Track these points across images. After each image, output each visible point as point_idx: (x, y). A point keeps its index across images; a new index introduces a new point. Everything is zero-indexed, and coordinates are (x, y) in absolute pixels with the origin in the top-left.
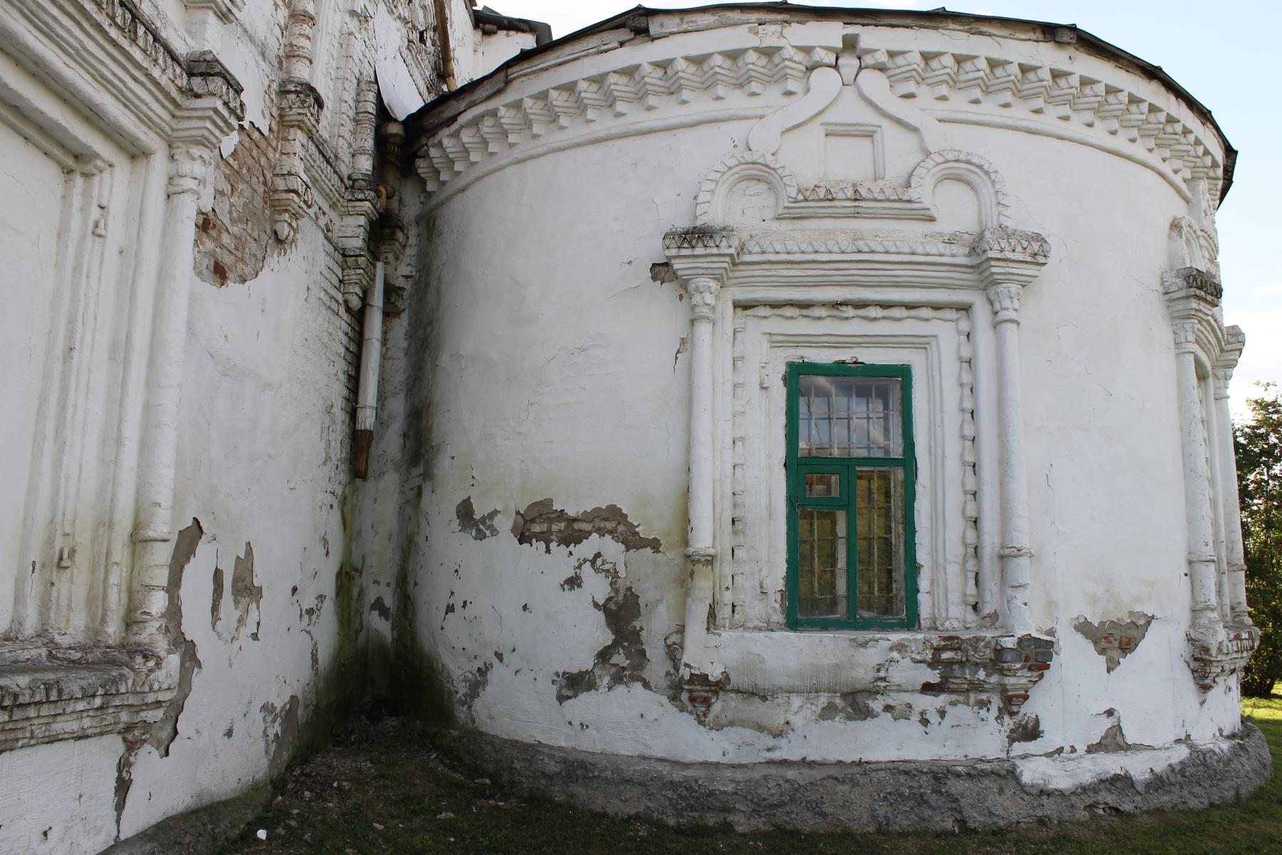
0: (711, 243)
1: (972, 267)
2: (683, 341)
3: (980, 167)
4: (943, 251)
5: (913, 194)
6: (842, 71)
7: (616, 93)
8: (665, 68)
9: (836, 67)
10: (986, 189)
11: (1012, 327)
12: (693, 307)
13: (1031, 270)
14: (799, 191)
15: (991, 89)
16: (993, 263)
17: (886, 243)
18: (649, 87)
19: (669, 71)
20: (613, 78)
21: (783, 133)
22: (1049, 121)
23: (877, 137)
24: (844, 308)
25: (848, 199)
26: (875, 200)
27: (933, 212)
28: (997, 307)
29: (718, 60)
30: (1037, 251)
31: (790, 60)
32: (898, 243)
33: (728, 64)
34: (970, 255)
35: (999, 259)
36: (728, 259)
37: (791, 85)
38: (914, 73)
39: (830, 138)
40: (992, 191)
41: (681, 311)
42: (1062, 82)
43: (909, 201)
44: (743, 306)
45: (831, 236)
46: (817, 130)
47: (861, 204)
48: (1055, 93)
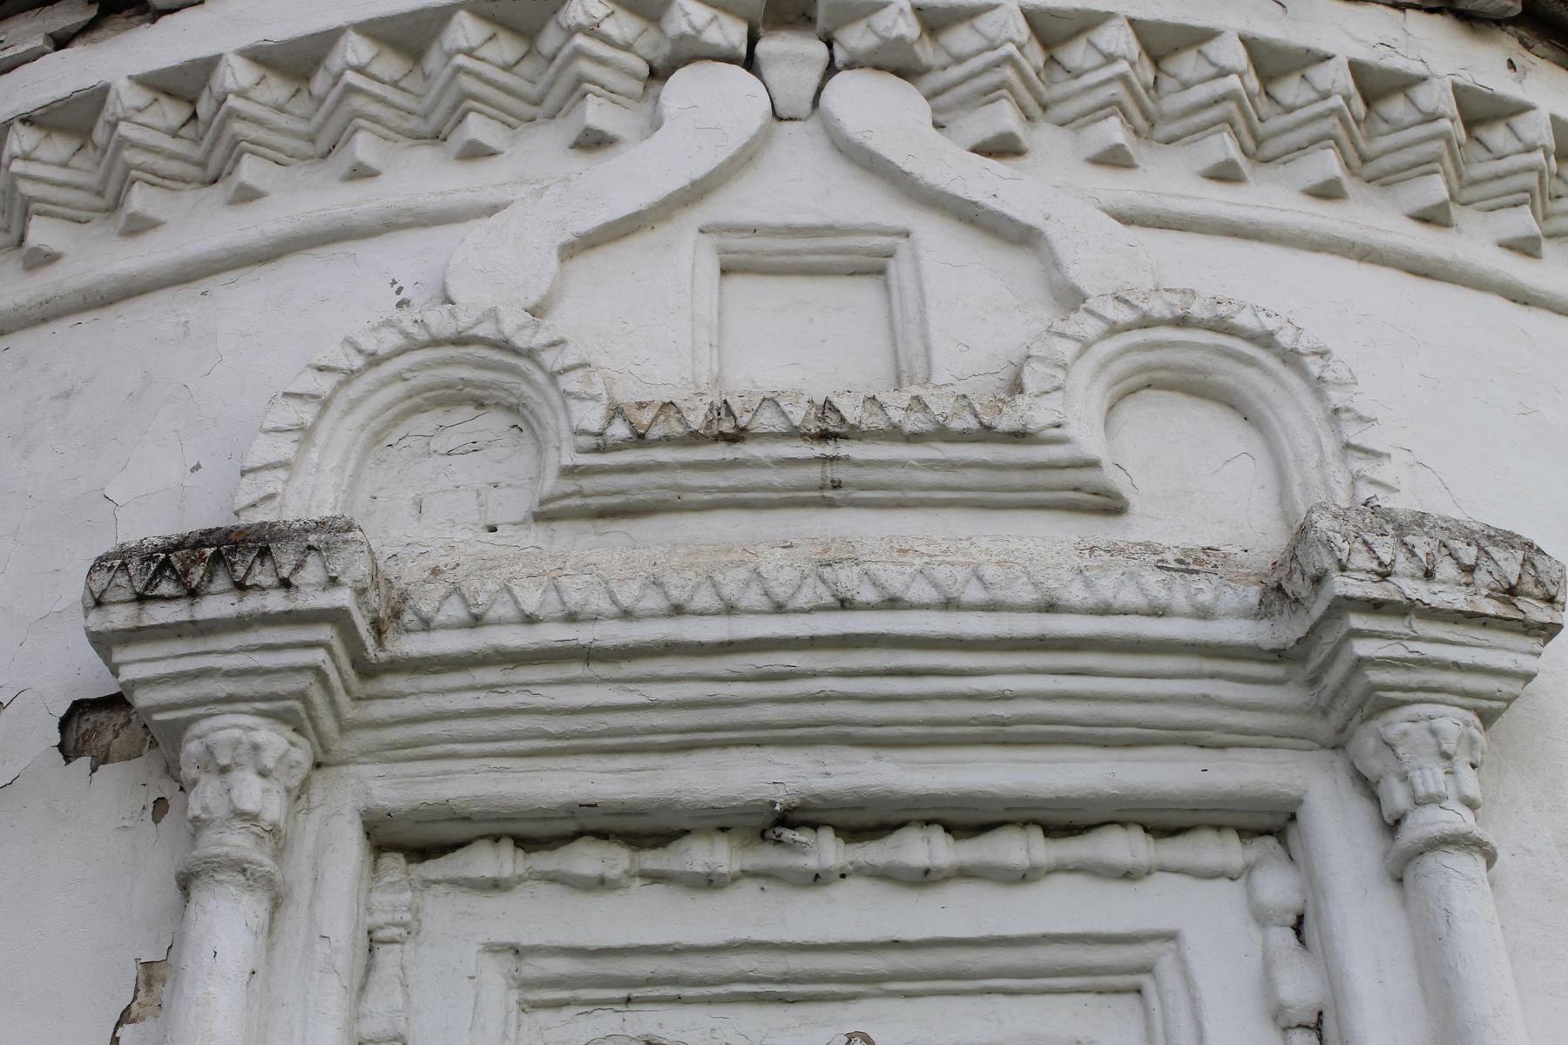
0: (262, 575)
1: (1278, 655)
2: (151, 975)
3: (1265, 340)
4: (1160, 594)
5: (1036, 412)
6: (771, 74)
7: (26, 188)
8: (193, 102)
9: (750, 63)
10: (1296, 415)
11: (1467, 865)
12: (198, 825)
13: (1505, 652)
14: (616, 411)
15: (1271, 148)
16: (1357, 621)
17: (941, 573)
18: (131, 156)
19: (204, 107)
22: (1474, 242)
23: (899, 269)
24: (802, 836)
25: (795, 434)
26: (893, 434)
27: (1112, 477)
28: (1397, 797)
29: (357, 50)
31: (592, 31)
32: (989, 572)
33: (391, 66)
34: (1262, 611)
35: (1375, 607)
36: (325, 633)
37: (597, 113)
38: (1008, 72)
39: (737, 283)
40: (1315, 412)
41: (158, 855)
42: (1497, 136)
43: (1019, 436)
44: (406, 842)
46: (685, 255)
48: (1478, 171)
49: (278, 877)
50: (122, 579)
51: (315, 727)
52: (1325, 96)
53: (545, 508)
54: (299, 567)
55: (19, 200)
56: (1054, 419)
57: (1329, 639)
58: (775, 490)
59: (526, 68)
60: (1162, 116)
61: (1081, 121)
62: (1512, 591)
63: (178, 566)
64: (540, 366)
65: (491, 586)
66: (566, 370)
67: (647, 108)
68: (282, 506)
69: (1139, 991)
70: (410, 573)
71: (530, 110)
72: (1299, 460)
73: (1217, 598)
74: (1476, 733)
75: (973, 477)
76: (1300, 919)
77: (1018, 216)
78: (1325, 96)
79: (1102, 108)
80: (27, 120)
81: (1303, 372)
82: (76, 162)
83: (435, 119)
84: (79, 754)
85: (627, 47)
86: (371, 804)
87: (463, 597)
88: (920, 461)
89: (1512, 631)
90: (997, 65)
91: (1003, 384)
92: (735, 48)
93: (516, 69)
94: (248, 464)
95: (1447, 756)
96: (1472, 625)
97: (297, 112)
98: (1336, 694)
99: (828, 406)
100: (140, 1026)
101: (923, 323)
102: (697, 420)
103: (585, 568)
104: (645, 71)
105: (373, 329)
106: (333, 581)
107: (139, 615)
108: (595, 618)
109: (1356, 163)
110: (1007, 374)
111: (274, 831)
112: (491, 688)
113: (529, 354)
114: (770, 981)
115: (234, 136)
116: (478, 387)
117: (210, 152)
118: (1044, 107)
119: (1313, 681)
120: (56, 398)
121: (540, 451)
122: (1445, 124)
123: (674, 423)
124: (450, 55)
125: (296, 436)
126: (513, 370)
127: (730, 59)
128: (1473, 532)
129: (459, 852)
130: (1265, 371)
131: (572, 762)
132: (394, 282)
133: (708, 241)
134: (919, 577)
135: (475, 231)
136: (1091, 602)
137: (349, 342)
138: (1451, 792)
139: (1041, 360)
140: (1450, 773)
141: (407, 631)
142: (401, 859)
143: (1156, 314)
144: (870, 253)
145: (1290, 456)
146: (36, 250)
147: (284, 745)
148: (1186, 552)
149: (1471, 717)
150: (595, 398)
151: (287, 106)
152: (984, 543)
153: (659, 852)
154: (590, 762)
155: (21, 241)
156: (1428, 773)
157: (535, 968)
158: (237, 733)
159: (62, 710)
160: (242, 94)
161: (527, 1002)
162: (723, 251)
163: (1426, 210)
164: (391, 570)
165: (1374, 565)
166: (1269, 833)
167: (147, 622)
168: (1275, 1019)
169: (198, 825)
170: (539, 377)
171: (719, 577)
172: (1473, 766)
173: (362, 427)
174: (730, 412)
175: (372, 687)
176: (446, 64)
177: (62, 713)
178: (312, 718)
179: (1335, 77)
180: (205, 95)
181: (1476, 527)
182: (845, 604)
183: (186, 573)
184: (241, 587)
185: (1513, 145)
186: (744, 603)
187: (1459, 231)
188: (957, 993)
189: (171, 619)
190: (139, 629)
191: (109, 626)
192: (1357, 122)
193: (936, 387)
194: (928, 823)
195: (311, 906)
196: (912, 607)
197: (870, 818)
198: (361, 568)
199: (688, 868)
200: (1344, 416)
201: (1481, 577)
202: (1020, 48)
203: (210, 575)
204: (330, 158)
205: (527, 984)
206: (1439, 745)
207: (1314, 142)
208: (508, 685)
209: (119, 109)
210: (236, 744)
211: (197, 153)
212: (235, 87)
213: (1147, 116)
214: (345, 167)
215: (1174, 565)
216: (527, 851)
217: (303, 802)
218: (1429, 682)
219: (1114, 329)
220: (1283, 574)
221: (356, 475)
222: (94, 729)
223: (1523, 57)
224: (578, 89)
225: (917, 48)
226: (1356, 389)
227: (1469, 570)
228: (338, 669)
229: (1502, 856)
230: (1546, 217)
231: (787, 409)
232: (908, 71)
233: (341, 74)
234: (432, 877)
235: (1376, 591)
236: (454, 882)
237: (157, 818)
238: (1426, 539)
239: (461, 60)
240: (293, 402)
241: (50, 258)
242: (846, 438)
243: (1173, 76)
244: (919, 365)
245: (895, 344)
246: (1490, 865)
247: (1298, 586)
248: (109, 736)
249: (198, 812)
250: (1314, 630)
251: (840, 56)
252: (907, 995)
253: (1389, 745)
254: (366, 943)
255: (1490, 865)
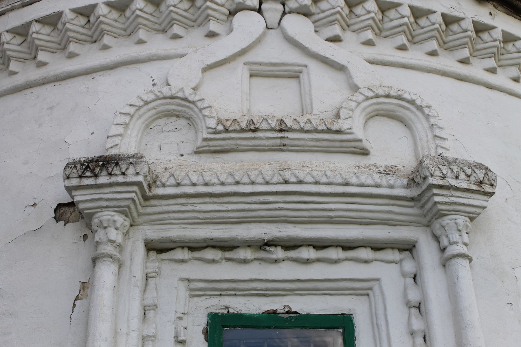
0: (116, 171)
1: (412, 199)
2: (84, 286)
3: (412, 102)
4: (379, 181)
5: (343, 124)
6: (266, 14)
7: (37, 42)
8: (88, 17)
9: (259, 11)
10: (421, 126)
11: (464, 262)
12: (97, 244)
13: (477, 200)
14: (219, 122)
15: (416, 39)
16: (435, 191)
17: (315, 173)
18: (70, 34)
19: (92, 19)
20: (35, 27)
21: (205, 70)
22: (476, 70)
23: (304, 77)
24: (272, 249)
25: (272, 130)
26: (302, 130)
27: (366, 144)
28: (445, 242)
30: (484, 185)
32: (329, 173)
34: (408, 186)
35: (441, 187)
36: (135, 188)
37: (213, 26)
39: (255, 80)
40: (426, 125)
41: (85, 252)
42: (485, 36)
43: (339, 132)
44: (157, 248)
45: (258, 167)
46: (239, 72)
47: (287, 135)
48: (479, 47)
49: (121, 259)
50: (75, 171)
51: (131, 215)
52: (434, 24)
53: (198, 150)
54: (127, 169)
55: (35, 45)
56: (349, 127)
57: (427, 195)
58: (266, 146)
59: (192, 10)
60: (384, 29)
61: (359, 31)
62: (481, 182)
63: (91, 168)
64: (197, 106)
65: (183, 174)
66: (204, 108)
67: (228, 24)
68: (120, 148)
69: (368, 295)
70: (158, 169)
71: (192, 24)
72: (421, 140)
73: (395, 182)
74: (468, 224)
75: (325, 143)
76: (415, 275)
77: (340, 62)
78: (434, 24)
79: (366, 27)
80: (37, 21)
81: (423, 113)
82: (52, 34)
83: (163, 25)
84: (60, 220)
85: (222, 6)
86: (147, 237)
87: (174, 177)
88: (309, 139)
89: (480, 194)
90: (335, 14)
91: (334, 114)
92: (255, 7)
93: (189, 11)
94: (110, 135)
95: (460, 231)
96: (469, 192)
97: (121, 21)
98: (428, 211)
99: (282, 121)
100: (81, 301)
101: (311, 95)
102: (243, 125)
103: (210, 169)
104: (228, 13)
105: (146, 93)
106: (138, 173)
107: (80, 182)
108: (213, 185)
109: (442, 44)
110: (335, 111)
111: (120, 245)
112: (182, 204)
113: (193, 103)
114: (262, 290)
115: (102, 29)
116: (177, 112)
117: (94, 33)
118: (348, 26)
119: (422, 207)
120: (48, 109)
121: (196, 132)
122: (469, 33)
123: (237, 126)
124: (168, 7)
125: (124, 126)
126: (188, 107)
127: (254, 10)
128: (471, 164)
129: (172, 251)
130: (412, 112)
131: (205, 226)
132: (152, 78)
133: (246, 67)
134: (308, 175)
135: (177, 62)
136: (358, 183)
137: (139, 97)
138: (460, 241)
139: (346, 108)
140: (460, 235)
141: (158, 187)
142: (155, 252)
143: (380, 94)
144: (295, 71)
145: (418, 138)
146: (40, 62)
147: (123, 221)
148: (386, 167)
149: (467, 219)
150: (213, 117)
151: (118, 20)
152: (327, 164)
153: (230, 252)
154: (211, 226)
155: (35, 58)
156: (454, 236)
157: (194, 285)
158: (109, 217)
159: (55, 206)
160: (104, 16)
161: (191, 295)
162: (250, 70)
163: (462, 59)
164: (153, 168)
165: (441, 175)
166: (407, 250)
167: (82, 184)
168: (407, 304)
169: (98, 244)
170: (196, 110)
171: (250, 173)
172: (467, 233)
173: (143, 123)
174: (253, 123)
175: (147, 203)
176: (167, 9)
177: (55, 207)
178: (130, 213)
179: (437, 18)
180: (93, 14)
181: (472, 163)
182: (286, 182)
183: (94, 170)
184: (110, 174)
185: (490, 39)
186: (257, 181)
187: (472, 65)
188: (315, 295)
189: (90, 183)
190: (80, 186)
191: (71, 185)
192: (443, 32)
193: (314, 115)
194: (308, 245)
195: (130, 267)
196: (306, 183)
197: (292, 244)
198: (146, 170)
199: (239, 257)
200: (434, 126)
201: (472, 178)
202: (342, 9)
203: (101, 170)
204: (131, 36)
205: (191, 290)
206: (458, 227)
207: (430, 38)
208: (188, 204)
209: (66, 19)
210: (109, 220)
211: (90, 33)
212: (102, 14)
213: (379, 29)
214: (136, 40)
215: (383, 172)
216: (192, 251)
217: (127, 237)
218: (456, 209)
219: (368, 98)
220: (415, 175)
221: (141, 138)
222: (64, 212)
223: (494, 11)
224: (207, 18)
225: (311, 8)
226: (439, 118)
227: (469, 176)
228: (138, 198)
229: (474, 259)
230: (499, 61)
231: (270, 122)
232: (307, 14)
233: (135, 11)
234: (164, 258)
235: (441, 182)
236: (170, 260)
237: (84, 241)
238: (456, 167)
239: (172, 8)
240: (122, 115)
241: (45, 64)
242: (287, 131)
243: (388, 17)
244: (309, 107)
245: (301, 100)
246: (470, 262)
247: (419, 179)
248: (69, 214)
249: (98, 240)
250: (423, 193)
251: (287, 9)
252: (301, 295)
253: (443, 227)
254: (145, 277)
255: (470, 262)
